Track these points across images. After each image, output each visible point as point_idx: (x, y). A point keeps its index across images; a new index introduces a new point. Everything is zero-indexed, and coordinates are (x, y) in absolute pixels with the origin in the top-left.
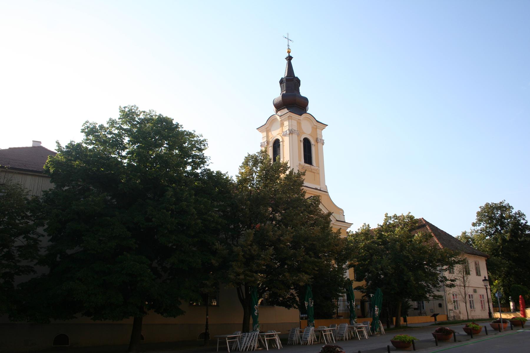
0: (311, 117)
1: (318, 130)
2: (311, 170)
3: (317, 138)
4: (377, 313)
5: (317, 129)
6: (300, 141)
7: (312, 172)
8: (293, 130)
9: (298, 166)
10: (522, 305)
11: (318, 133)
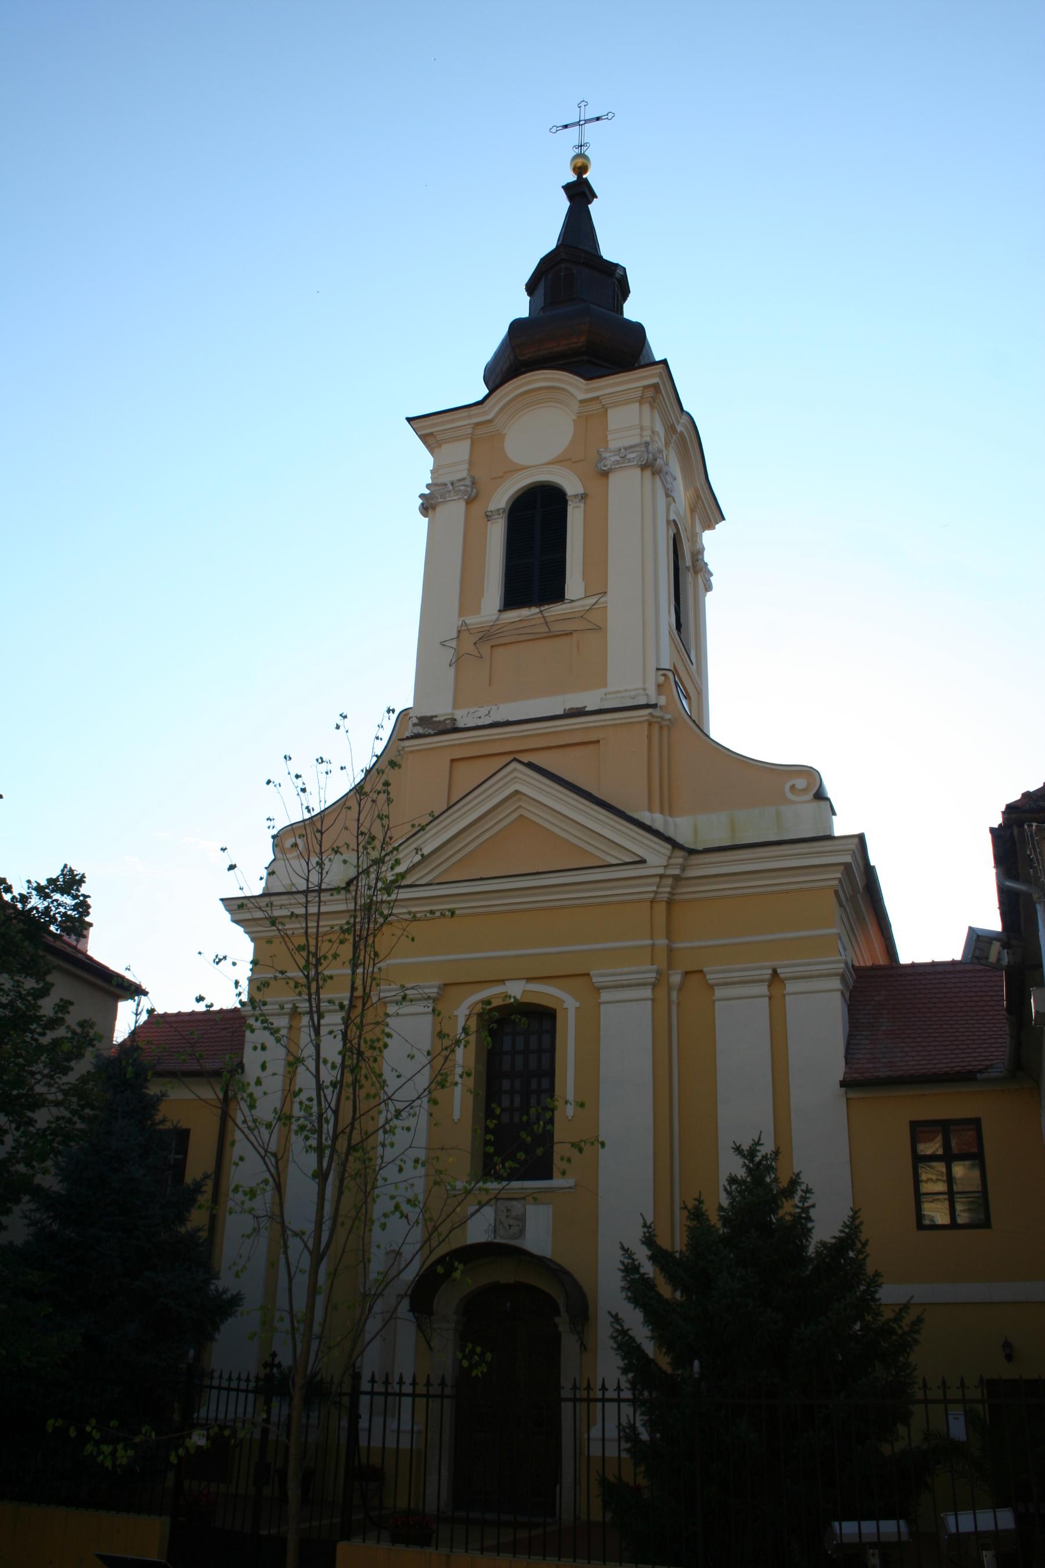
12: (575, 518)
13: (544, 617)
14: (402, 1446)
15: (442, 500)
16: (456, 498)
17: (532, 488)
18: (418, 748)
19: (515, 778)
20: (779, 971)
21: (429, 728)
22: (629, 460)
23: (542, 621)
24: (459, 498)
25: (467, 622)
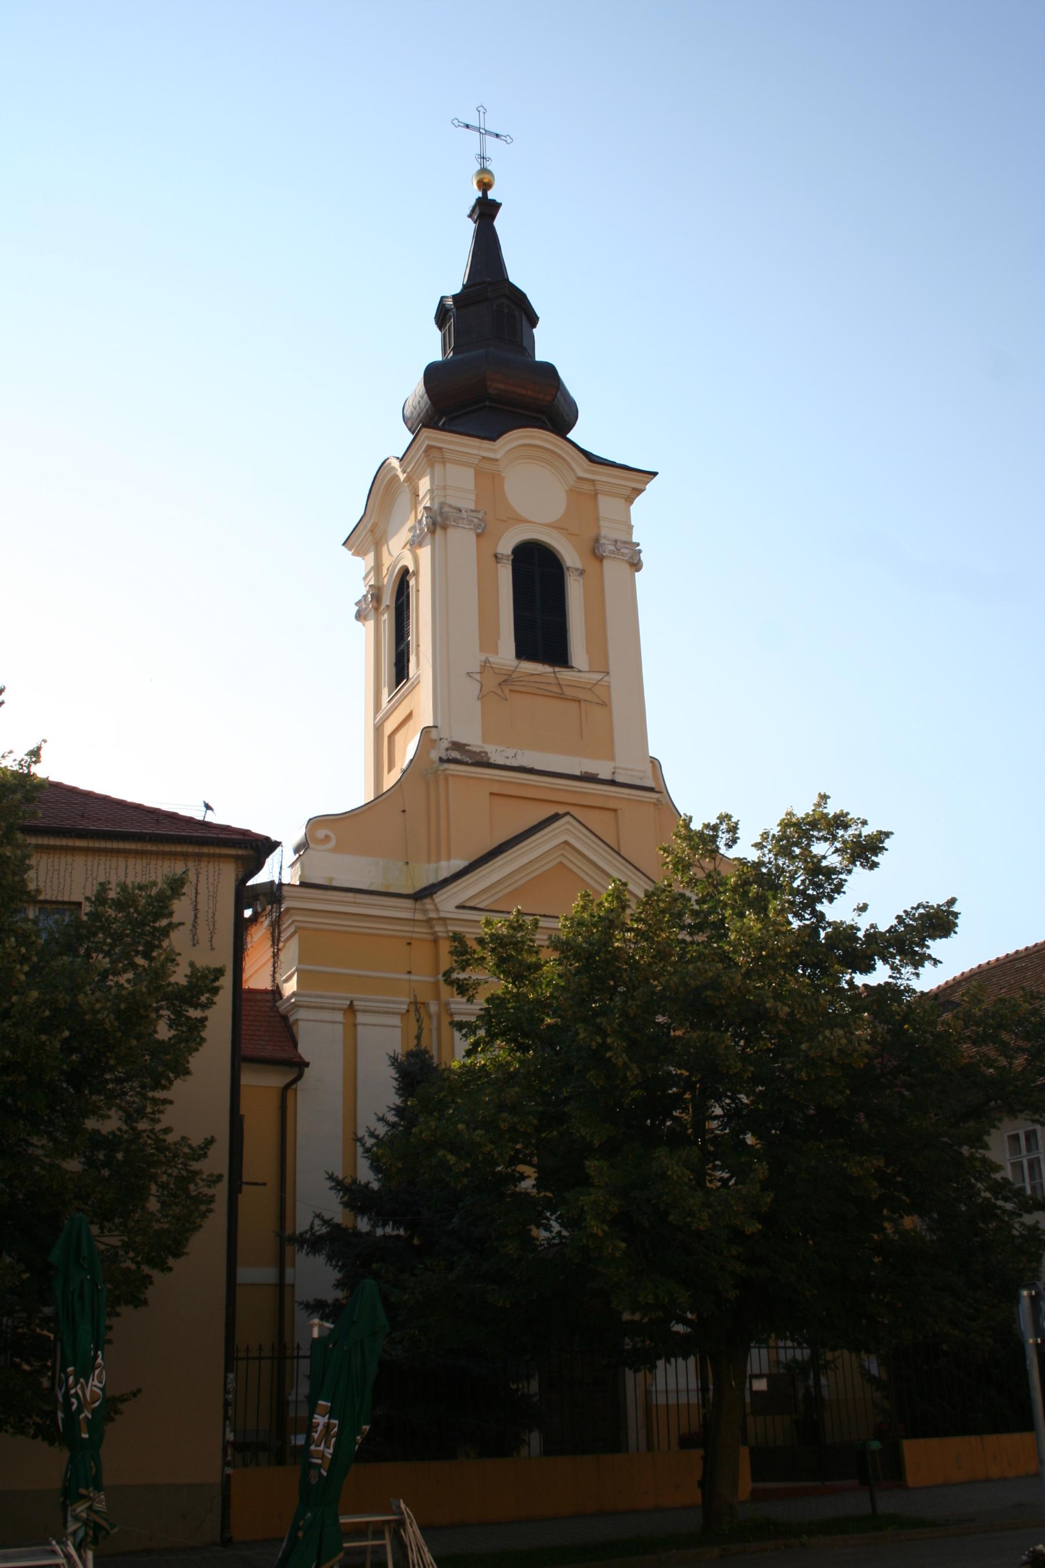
0: (558, 446)
1: (606, 505)
2: (557, 690)
3: (597, 540)
4: (323, 1457)
5: (600, 497)
6: (496, 556)
7: (562, 697)
8: (446, 509)
9: (478, 677)
10: (338, 1429)
11: (602, 514)
12: (575, 591)
13: (557, 678)
14: (670, 1402)
15: (454, 524)
16: (468, 527)
17: (540, 545)
18: (459, 773)
19: (567, 829)
20: (355, 1003)
21: (466, 756)
22: (623, 554)
23: (555, 681)
24: (471, 529)
25: (491, 659)
